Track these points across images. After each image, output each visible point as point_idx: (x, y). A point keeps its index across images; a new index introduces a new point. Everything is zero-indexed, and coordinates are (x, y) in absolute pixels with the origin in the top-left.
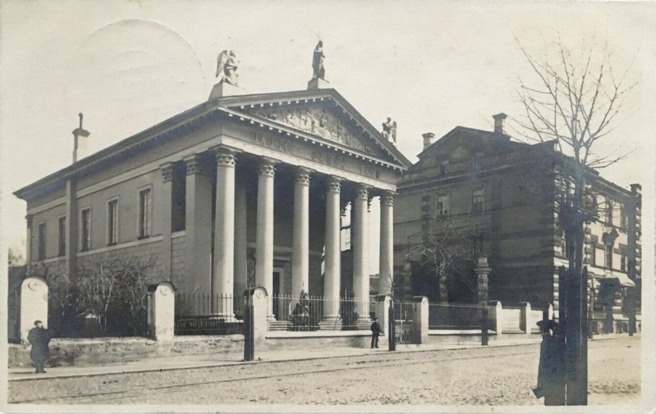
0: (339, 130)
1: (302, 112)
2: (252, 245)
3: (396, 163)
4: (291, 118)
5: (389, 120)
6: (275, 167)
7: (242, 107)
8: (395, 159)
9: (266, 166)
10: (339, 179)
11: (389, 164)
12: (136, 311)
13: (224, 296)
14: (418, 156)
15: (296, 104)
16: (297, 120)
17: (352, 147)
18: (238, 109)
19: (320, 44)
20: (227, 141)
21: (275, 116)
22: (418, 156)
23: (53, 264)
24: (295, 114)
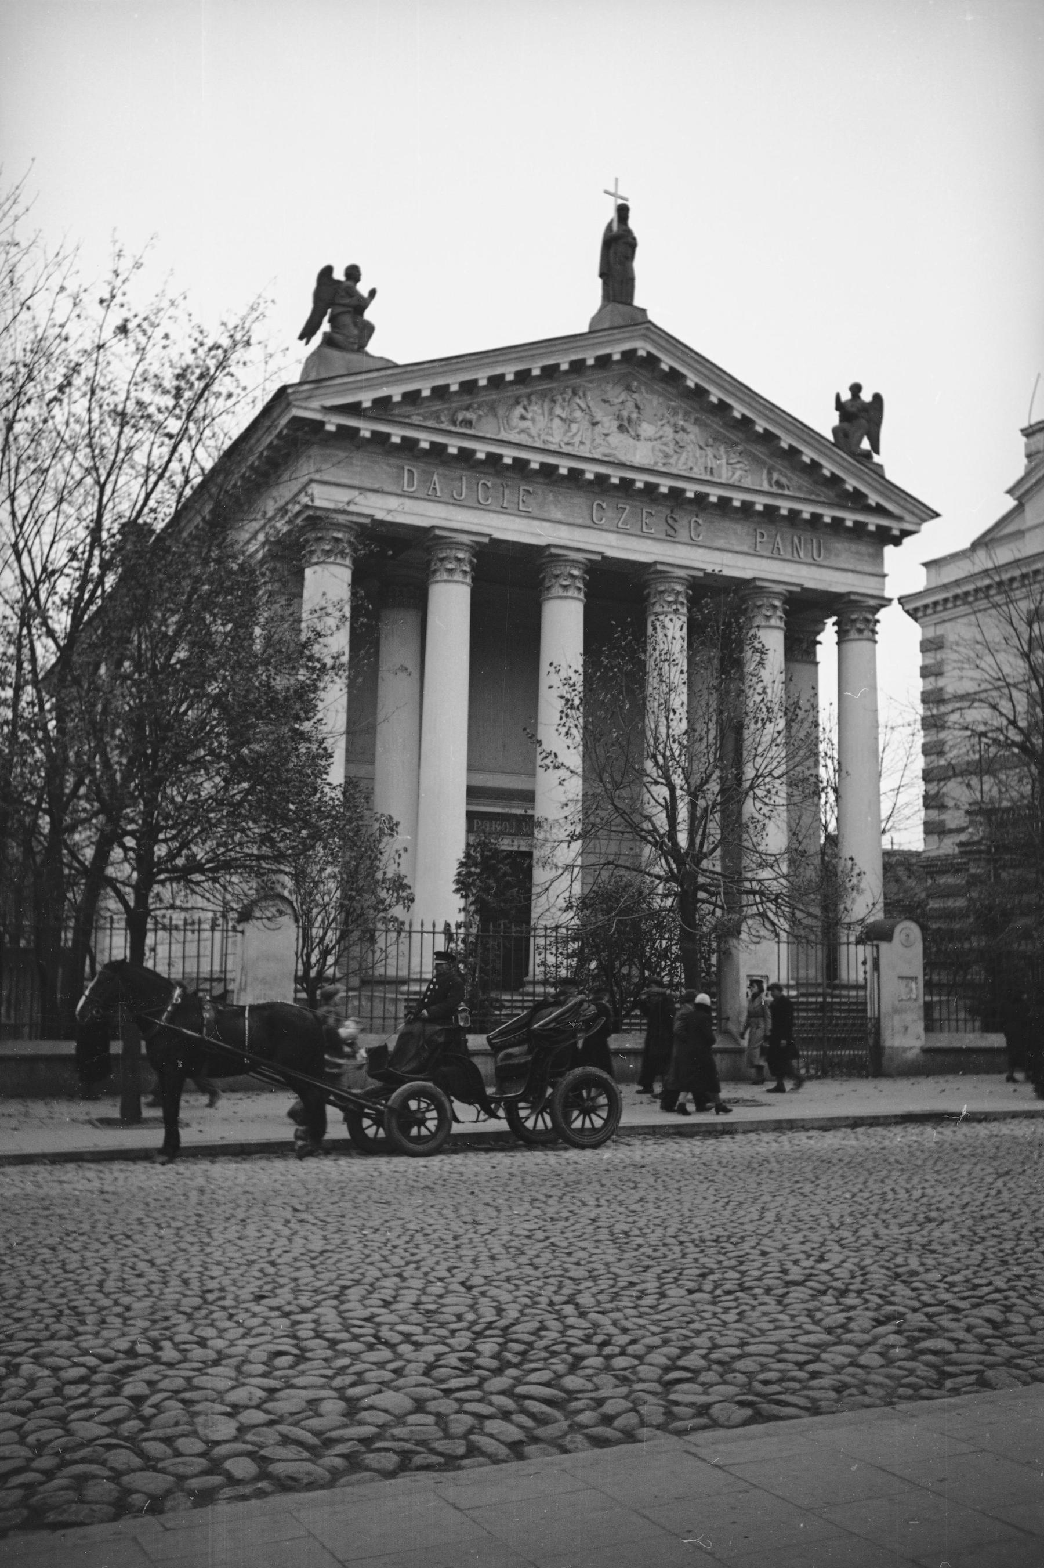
0: (680, 436)
1: (559, 398)
2: (362, 771)
3: (880, 510)
4: (523, 418)
5: (856, 389)
6: (785, 603)
7: (367, 404)
8: (873, 499)
9: (854, 616)
10: (465, 539)
11: (850, 518)
12: (756, 1003)
13: (417, 927)
14: (1010, 492)
15: (539, 374)
16: (542, 421)
17: (723, 481)
18: (353, 409)
19: (623, 212)
20: (324, 497)
21: (470, 415)
22: (1010, 492)
23: (234, 863)
24: (535, 408)
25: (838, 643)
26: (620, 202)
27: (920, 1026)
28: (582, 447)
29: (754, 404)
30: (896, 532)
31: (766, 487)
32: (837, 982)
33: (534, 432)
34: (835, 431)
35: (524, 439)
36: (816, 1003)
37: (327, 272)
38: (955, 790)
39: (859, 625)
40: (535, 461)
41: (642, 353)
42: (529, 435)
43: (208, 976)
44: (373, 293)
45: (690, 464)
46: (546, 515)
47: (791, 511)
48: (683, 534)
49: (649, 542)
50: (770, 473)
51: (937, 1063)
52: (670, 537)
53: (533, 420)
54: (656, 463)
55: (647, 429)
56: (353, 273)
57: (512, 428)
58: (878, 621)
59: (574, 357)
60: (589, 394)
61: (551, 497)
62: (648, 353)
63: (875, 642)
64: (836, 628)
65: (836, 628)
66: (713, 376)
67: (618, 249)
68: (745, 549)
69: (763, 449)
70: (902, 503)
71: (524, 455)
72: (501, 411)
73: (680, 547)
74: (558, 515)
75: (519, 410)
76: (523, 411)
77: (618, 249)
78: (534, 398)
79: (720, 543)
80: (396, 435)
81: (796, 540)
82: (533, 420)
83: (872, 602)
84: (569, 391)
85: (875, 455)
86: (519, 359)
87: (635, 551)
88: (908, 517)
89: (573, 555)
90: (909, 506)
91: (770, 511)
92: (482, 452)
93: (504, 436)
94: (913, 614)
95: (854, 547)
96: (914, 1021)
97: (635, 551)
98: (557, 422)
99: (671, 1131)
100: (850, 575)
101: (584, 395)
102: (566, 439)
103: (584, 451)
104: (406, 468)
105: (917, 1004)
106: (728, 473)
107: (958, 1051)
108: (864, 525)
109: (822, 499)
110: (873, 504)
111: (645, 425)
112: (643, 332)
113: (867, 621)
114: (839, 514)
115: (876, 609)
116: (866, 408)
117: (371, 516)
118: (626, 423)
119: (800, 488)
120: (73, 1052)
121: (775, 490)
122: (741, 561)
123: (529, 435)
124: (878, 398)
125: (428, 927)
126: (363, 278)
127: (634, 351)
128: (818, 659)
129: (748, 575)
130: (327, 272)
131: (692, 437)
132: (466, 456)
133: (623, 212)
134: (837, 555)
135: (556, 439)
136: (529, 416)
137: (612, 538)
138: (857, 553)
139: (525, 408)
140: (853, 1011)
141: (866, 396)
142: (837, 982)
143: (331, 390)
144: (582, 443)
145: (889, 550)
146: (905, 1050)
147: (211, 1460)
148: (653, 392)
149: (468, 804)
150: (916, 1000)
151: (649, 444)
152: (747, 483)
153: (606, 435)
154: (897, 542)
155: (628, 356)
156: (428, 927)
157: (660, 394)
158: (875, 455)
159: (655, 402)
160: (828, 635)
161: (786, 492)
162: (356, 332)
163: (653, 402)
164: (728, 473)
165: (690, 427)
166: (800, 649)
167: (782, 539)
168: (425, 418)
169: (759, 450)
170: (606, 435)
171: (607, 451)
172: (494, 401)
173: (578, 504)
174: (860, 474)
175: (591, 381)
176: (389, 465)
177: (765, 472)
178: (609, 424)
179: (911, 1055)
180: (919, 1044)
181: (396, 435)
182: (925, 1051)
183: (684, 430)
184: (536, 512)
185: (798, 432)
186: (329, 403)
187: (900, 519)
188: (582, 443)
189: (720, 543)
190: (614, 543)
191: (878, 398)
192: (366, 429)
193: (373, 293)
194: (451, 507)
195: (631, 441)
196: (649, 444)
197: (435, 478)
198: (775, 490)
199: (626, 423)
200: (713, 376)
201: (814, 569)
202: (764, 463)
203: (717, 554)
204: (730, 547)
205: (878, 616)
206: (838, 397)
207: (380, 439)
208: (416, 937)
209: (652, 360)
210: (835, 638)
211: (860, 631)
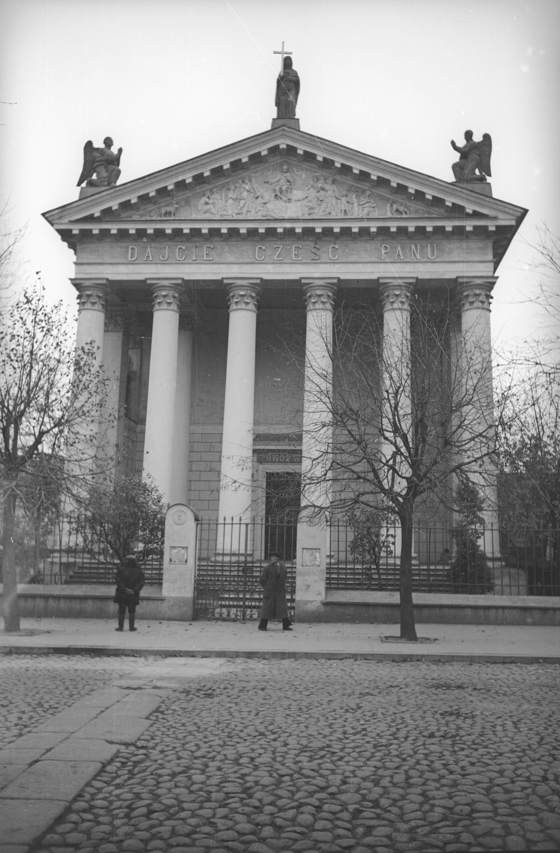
1: (232, 187)
4: (207, 203)
5: (469, 135)
18: (90, 219)
19: (287, 63)
26: (285, 55)
27: (322, 586)
28: (249, 214)
29: (365, 161)
31: (389, 215)
33: (213, 210)
34: (456, 168)
35: (208, 216)
36: (443, 570)
37: (89, 146)
39: (471, 299)
40: (205, 229)
41: (283, 146)
42: (212, 213)
43: (229, 552)
44: (120, 150)
45: (328, 210)
46: (223, 261)
48: (324, 258)
49: (297, 266)
50: (391, 205)
51: (332, 614)
52: (315, 261)
53: (213, 203)
54: (303, 215)
55: (297, 194)
56: (108, 142)
57: (199, 211)
59: (232, 160)
60: (254, 180)
61: (227, 249)
62: (288, 145)
63: (490, 311)
66: (333, 150)
67: (288, 85)
68: (374, 259)
69: (384, 191)
70: (495, 206)
71: (197, 226)
72: (193, 202)
73: (321, 265)
74: (232, 259)
75: (205, 199)
76: (207, 200)
77: (288, 85)
78: (215, 190)
79: (354, 258)
80: (132, 229)
81: (413, 247)
82: (213, 203)
84: (240, 181)
85: (487, 177)
86: (195, 168)
87: (287, 273)
88: (501, 216)
89: (239, 282)
90: (500, 208)
91: (402, 231)
92: (186, 228)
93: (194, 217)
95: (464, 245)
96: (315, 581)
97: (287, 273)
98: (230, 201)
99: (46, 651)
100: (461, 264)
101: (250, 181)
102: (236, 211)
103: (250, 216)
104: (130, 247)
105: (319, 569)
106: (361, 211)
107: (367, 605)
110: (471, 212)
111: (295, 192)
112: (280, 133)
116: (477, 146)
117: (107, 279)
118: (278, 193)
119: (416, 211)
120: (414, 594)
121: (396, 215)
122: (370, 268)
123: (212, 213)
124: (487, 137)
125: (229, 521)
126: (114, 142)
127: (277, 147)
129: (374, 277)
130: (89, 146)
131: (329, 193)
132: (178, 232)
133: (287, 63)
134: (449, 253)
135: (231, 211)
136: (210, 202)
137: (270, 268)
138: (468, 248)
139: (209, 198)
140: (438, 575)
141: (477, 138)
143: (73, 210)
144: (248, 212)
146: (307, 602)
147: (113, 827)
148: (302, 170)
149: (254, 445)
150: (319, 566)
151: (297, 202)
152: (376, 215)
153: (265, 203)
155: (284, 149)
156: (229, 521)
157: (307, 170)
158: (487, 177)
159: (304, 176)
161: (404, 216)
162: (106, 175)
163: (302, 175)
164: (361, 211)
165: (327, 187)
167: (402, 248)
168: (142, 216)
169: (383, 192)
170: (265, 203)
171: (264, 214)
172: (188, 197)
173: (247, 250)
174: (455, 192)
175: (256, 172)
176: (120, 247)
177: (389, 205)
178: (268, 196)
179: (311, 607)
180: (322, 597)
181: (132, 229)
182: (326, 604)
183: (323, 189)
184: (216, 260)
185: (402, 174)
186: (74, 218)
187: (495, 218)
188: (248, 212)
189: (354, 258)
190: (272, 271)
191: (487, 137)
192: (95, 229)
193: (120, 150)
194: (159, 266)
195: (283, 204)
196: (297, 202)
197: (149, 250)
198: (396, 215)
199: (278, 193)
200: (333, 150)
201: (429, 265)
202: (388, 200)
203: (350, 266)
204: (361, 260)
206: (453, 143)
207: (105, 233)
208: (221, 527)
209: (291, 150)
211: (472, 303)
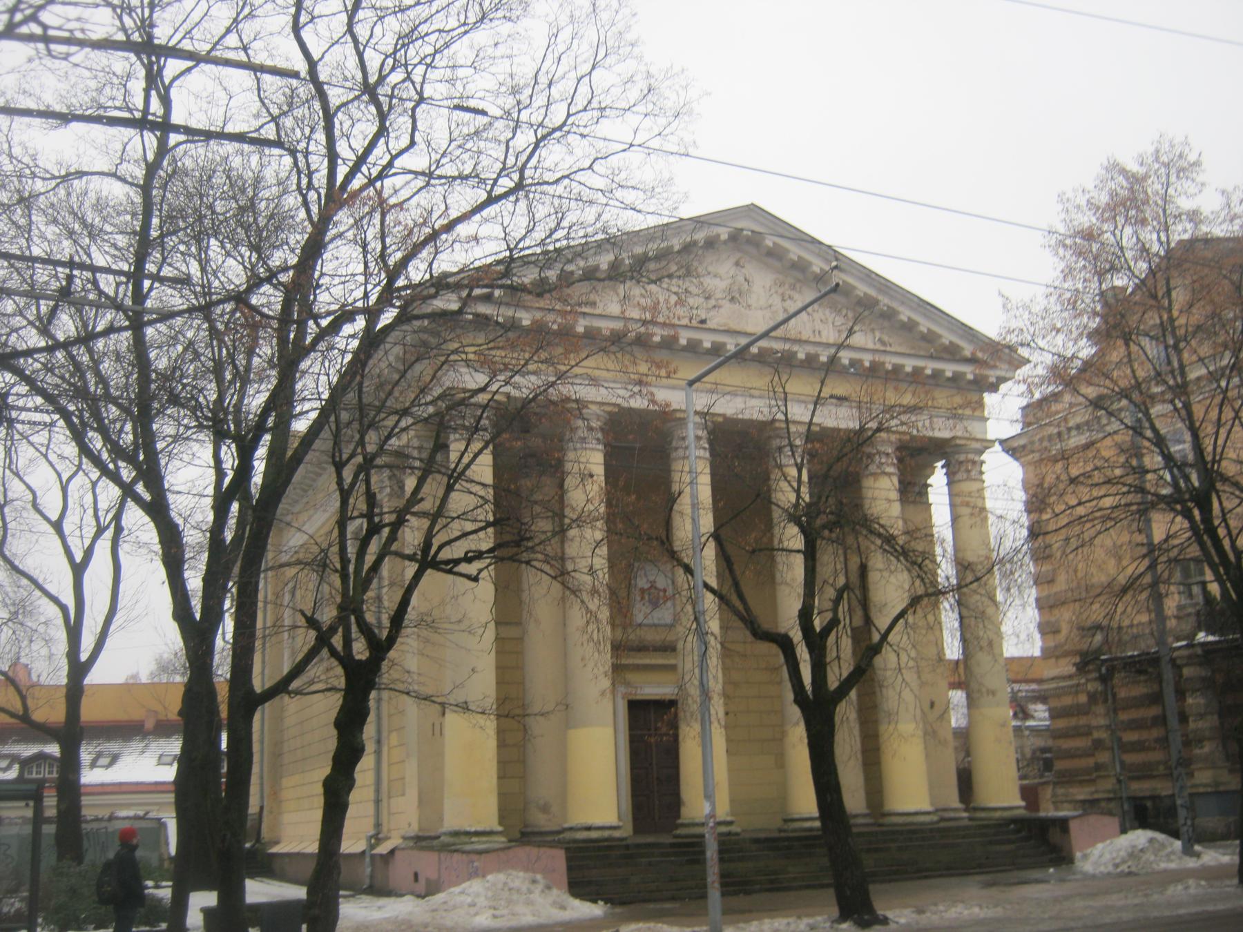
11: (949, 369)
25: (948, 484)
30: (992, 380)
31: (870, 346)
32: (680, 821)
38: (1066, 616)
47: (873, 363)
58: (983, 462)
64: (944, 470)
65: (944, 470)
83: (977, 445)
94: (1006, 451)
108: (941, 372)
109: (922, 353)
113: (974, 462)
114: (920, 363)
115: (981, 452)
128: (930, 501)
142: (680, 821)
145: (989, 398)
154: (994, 388)
160: (938, 480)
161: (888, 349)
166: (913, 490)
205: (983, 457)
210: (945, 480)
